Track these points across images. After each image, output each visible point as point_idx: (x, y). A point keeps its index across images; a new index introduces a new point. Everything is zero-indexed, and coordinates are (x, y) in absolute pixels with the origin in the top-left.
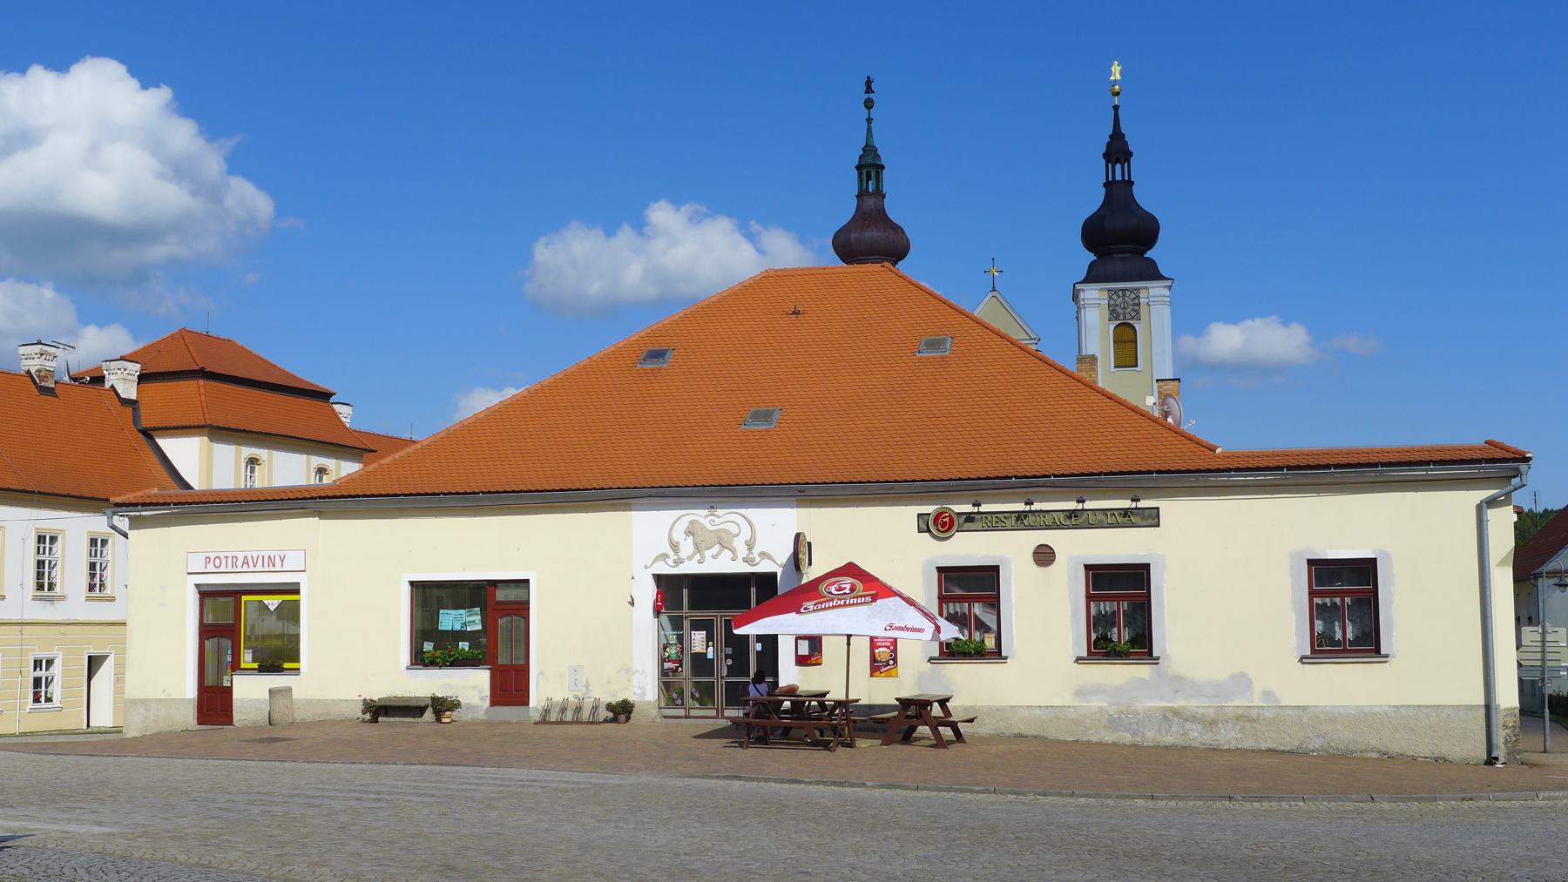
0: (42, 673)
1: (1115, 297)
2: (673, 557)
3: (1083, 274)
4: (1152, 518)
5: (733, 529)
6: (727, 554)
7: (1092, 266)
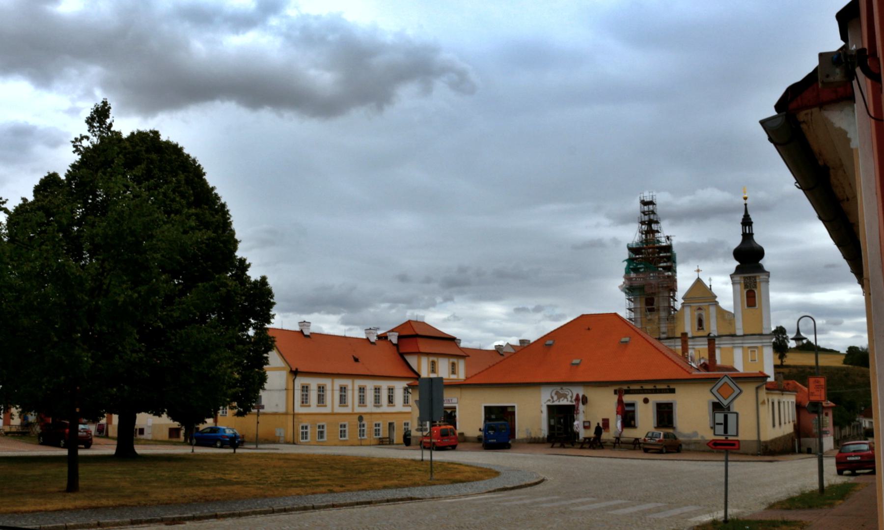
0: (362, 428)
2: (552, 400)
3: (700, 277)
4: (672, 391)
5: (567, 393)
6: (566, 400)
7: (738, 268)
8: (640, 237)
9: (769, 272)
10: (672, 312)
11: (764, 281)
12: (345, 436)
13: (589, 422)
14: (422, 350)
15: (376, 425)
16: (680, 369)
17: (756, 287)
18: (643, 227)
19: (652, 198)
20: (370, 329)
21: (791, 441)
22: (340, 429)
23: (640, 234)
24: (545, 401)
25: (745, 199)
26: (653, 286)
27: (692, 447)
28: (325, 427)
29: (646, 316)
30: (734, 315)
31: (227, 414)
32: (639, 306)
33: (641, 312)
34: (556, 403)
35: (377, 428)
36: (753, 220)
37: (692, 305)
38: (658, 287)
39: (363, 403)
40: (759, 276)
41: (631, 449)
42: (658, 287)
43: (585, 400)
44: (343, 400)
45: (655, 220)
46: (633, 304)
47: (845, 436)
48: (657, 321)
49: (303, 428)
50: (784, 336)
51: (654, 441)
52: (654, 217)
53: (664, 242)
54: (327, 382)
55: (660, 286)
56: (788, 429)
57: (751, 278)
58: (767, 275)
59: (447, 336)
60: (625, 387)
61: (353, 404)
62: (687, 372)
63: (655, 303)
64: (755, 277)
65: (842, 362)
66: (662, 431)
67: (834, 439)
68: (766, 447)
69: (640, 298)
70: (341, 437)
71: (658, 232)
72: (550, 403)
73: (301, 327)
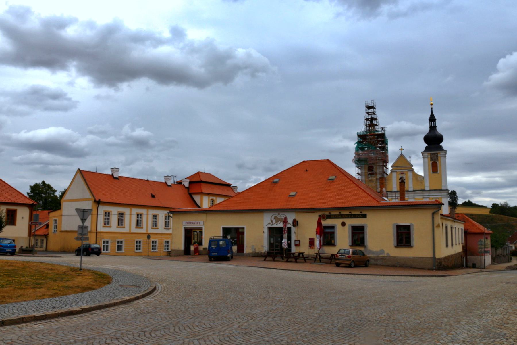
1: (432, 155)
3: (402, 153)
4: (364, 216)
7: (426, 148)
8: (365, 128)
9: (446, 151)
10: (385, 176)
11: (442, 156)
12: (107, 250)
13: (299, 241)
14: (204, 191)
15: (165, 242)
16: (371, 198)
17: (438, 160)
18: (368, 122)
19: (373, 104)
20: (168, 176)
21: (460, 257)
22: (136, 244)
23: (366, 127)
24: (267, 224)
25: (432, 104)
26: (373, 159)
27: (379, 262)
28: (124, 242)
29: (368, 178)
30: (424, 177)
31: (57, 232)
32: (364, 172)
33: (365, 175)
34: (275, 226)
35: (167, 244)
36: (436, 118)
37: (397, 171)
38: (376, 160)
39: (156, 226)
40: (440, 153)
41: (327, 263)
42: (376, 160)
43: (295, 223)
44: (138, 223)
45: (375, 117)
46: (360, 170)
47: (499, 255)
48: (375, 180)
49: (104, 242)
50: (456, 196)
51: (345, 257)
52: (374, 116)
53: (380, 131)
54: (126, 211)
55: (378, 159)
56: (458, 249)
57: (435, 154)
58: (444, 152)
59: (225, 183)
60: (327, 213)
61: (147, 226)
62: (377, 201)
63: (374, 170)
64: (437, 153)
65: (489, 212)
66: (351, 249)
67: (492, 257)
68: (440, 263)
69: (365, 166)
70: (137, 249)
71: (376, 125)
72: (270, 226)
73: (112, 172)
